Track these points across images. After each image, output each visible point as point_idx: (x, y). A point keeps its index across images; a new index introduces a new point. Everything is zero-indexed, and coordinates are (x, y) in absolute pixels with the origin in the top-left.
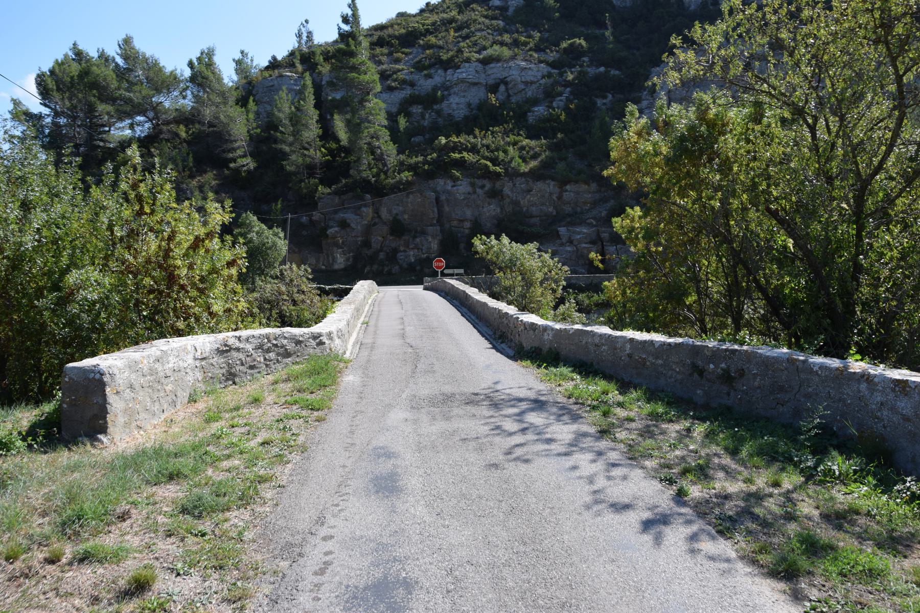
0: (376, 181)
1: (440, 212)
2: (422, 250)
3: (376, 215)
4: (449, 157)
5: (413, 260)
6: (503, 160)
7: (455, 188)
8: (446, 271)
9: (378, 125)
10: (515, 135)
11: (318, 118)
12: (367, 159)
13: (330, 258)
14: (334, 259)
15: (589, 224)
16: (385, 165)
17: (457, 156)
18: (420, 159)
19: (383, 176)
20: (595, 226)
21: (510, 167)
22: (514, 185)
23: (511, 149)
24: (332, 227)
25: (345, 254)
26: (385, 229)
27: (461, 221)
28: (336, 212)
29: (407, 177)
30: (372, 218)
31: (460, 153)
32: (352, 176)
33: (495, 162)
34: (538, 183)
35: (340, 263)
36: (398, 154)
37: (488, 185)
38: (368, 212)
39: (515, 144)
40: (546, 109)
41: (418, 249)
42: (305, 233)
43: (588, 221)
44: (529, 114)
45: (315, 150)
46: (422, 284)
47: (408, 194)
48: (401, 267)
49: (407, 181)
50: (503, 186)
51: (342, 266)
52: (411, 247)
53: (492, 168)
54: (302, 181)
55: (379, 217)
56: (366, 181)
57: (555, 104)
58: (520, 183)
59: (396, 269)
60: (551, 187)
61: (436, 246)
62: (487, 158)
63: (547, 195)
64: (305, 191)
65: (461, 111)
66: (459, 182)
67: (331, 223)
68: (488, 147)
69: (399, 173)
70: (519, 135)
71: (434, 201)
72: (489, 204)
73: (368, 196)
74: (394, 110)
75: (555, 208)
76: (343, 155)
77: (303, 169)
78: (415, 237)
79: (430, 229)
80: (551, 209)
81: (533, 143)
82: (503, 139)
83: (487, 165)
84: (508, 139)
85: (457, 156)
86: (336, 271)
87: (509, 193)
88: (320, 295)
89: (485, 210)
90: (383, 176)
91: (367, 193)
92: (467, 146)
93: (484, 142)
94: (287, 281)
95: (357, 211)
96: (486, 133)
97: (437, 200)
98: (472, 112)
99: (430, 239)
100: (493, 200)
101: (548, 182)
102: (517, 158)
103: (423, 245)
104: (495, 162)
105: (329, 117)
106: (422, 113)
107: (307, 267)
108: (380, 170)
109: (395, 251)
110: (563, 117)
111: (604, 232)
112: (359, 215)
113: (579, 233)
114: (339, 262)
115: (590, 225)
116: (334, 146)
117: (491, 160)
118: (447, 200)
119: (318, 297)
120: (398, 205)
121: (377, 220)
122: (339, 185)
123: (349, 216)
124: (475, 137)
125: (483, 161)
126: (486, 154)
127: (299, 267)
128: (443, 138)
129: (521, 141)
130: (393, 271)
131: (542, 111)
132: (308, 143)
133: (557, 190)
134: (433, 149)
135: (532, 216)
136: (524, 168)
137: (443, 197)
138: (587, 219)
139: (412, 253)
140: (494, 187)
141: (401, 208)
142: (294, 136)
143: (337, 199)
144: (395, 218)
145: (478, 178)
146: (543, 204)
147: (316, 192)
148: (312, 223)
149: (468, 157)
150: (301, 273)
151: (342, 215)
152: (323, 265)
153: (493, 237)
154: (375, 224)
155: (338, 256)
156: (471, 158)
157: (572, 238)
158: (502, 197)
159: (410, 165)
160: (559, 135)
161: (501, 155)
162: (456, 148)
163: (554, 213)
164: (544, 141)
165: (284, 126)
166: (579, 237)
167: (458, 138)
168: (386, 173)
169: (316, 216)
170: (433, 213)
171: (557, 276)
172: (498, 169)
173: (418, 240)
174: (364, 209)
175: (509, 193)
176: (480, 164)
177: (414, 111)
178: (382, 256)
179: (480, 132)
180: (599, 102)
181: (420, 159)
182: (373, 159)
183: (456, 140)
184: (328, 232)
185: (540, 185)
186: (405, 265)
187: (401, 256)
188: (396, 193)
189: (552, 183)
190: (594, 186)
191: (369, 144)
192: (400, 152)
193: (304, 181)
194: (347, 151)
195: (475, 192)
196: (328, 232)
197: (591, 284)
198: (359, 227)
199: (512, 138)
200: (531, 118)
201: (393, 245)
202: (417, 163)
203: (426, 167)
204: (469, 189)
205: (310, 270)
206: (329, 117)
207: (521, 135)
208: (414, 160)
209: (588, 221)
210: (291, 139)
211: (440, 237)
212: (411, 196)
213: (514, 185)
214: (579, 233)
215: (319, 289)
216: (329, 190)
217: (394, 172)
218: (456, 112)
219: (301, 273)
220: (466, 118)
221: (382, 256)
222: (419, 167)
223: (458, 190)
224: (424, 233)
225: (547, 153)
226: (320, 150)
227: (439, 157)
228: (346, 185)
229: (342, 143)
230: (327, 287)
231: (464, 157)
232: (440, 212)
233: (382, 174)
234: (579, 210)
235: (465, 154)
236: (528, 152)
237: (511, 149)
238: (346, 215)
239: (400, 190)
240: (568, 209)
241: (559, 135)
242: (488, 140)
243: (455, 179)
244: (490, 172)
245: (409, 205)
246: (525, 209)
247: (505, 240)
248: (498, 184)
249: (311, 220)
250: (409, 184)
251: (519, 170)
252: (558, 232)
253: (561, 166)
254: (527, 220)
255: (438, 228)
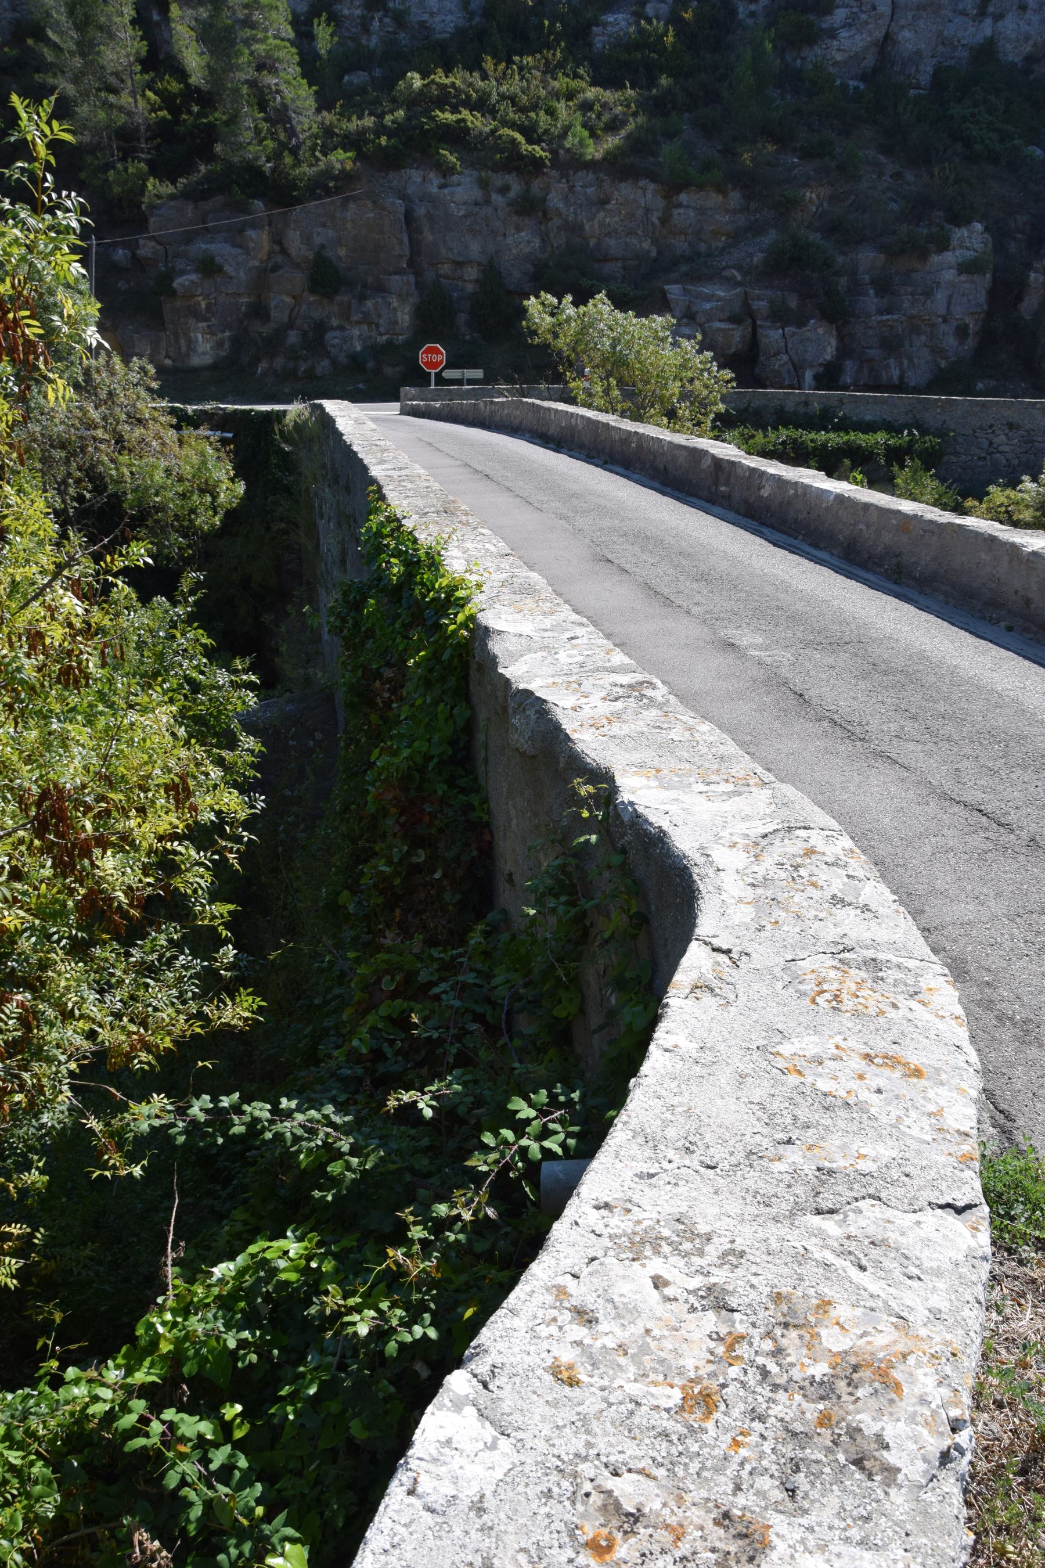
0: (274, 170)
1: (415, 245)
2: (377, 325)
3: (277, 248)
4: (432, 119)
5: (359, 348)
6: (546, 131)
7: (446, 191)
8: (448, 374)
9: (275, 37)
10: (568, 76)
11: (133, 13)
12: (250, 119)
13: (182, 342)
14: (191, 343)
15: (729, 279)
16: (292, 133)
17: (447, 117)
18: (369, 122)
19: (288, 160)
20: (739, 284)
21: (562, 147)
22: (571, 188)
23: (561, 106)
24: (183, 273)
25: (213, 334)
26: (298, 279)
27: (459, 264)
28: (189, 238)
29: (342, 162)
30: (270, 254)
31: (455, 110)
32: (219, 157)
33: (530, 133)
34: (623, 185)
35: (204, 353)
36: (318, 110)
37: (516, 187)
38: (260, 239)
39: (570, 96)
40: (632, 20)
41: (370, 324)
42: (122, 285)
43: (726, 273)
44: (595, 29)
45: (133, 94)
46: (394, 397)
47: (346, 200)
48: (334, 363)
49: (343, 171)
50: (547, 190)
51: (208, 360)
52: (355, 318)
53: (525, 148)
54: (108, 167)
55: (284, 251)
56: (253, 170)
57: (649, 10)
58: (584, 183)
59: (323, 366)
60: (649, 196)
61: (407, 318)
62: (513, 125)
63: (640, 213)
64: (117, 189)
65: (449, 17)
66: (455, 178)
67: (180, 264)
68: (513, 99)
69: (325, 155)
70: (576, 76)
71: (402, 218)
72: (519, 229)
73: (258, 204)
74: (303, 8)
75: (655, 242)
76: (196, 109)
77: (109, 138)
78: (362, 298)
79: (396, 282)
80: (646, 245)
81: (608, 95)
82: (545, 84)
83: (515, 140)
84: (556, 84)
85: (447, 117)
86: (195, 371)
87: (561, 205)
88: (178, 427)
89: (509, 240)
90: (288, 160)
91: (255, 196)
92: (468, 97)
93: (504, 88)
94: (103, 395)
95: (236, 236)
96: (507, 68)
97: (409, 217)
98: (471, 19)
99: (395, 304)
100: (527, 221)
101: (642, 183)
102: (579, 128)
103: (379, 316)
104: (530, 133)
105: (156, 17)
106: (363, 17)
107: (144, 362)
108: (283, 146)
109: (321, 328)
110: (670, 39)
111: (759, 299)
112: (240, 246)
113: (709, 298)
114: (201, 350)
115: (732, 283)
116: (175, 87)
117: (522, 130)
118: (430, 217)
119: (172, 432)
120: (324, 225)
121: (279, 259)
122: (194, 178)
123: (220, 249)
124: (485, 77)
125: (506, 131)
126: (511, 115)
127: (126, 361)
128: (417, 75)
129: (583, 91)
130: (319, 371)
131: (623, 24)
132: (116, 74)
133: (660, 203)
134: (394, 100)
135: (606, 259)
136: (594, 151)
137: (421, 211)
138: (725, 268)
139: (356, 332)
140: (528, 191)
141: (331, 233)
142: (83, 55)
143: (190, 209)
144: (319, 255)
145: (495, 170)
146: (631, 233)
147: (142, 194)
148: (138, 263)
149: (476, 122)
150: (134, 377)
151: (204, 246)
152: (168, 356)
153: (569, 298)
154: (275, 268)
155: (200, 336)
156: (478, 124)
157: (694, 309)
158: (545, 213)
159: (347, 136)
160: (664, 81)
161: (543, 119)
162: (446, 99)
163: (654, 254)
164: (630, 92)
165: (56, 26)
166: (708, 306)
167: (447, 77)
168: (294, 152)
169: (147, 248)
170: (399, 247)
171: (705, 392)
172: (538, 151)
173: (369, 304)
174: (251, 233)
175: (561, 205)
176: (500, 137)
177: (346, 12)
178: (293, 337)
179: (495, 65)
180: (741, 10)
181: (369, 122)
182: (265, 120)
183: (447, 81)
184: (175, 285)
185: (626, 190)
186: (342, 359)
187: (332, 338)
188: (320, 198)
189: (652, 186)
190: (735, 197)
191: (252, 84)
192: (324, 104)
193: (114, 168)
194: (206, 99)
195: (488, 201)
196: (175, 285)
197: (746, 409)
198: (242, 274)
199: (561, 83)
200: (600, 40)
201: (317, 315)
202: (363, 132)
203: (383, 141)
204: (477, 194)
205: (152, 370)
206: (156, 17)
207: (582, 78)
208: (354, 125)
209: (726, 273)
210: (78, 62)
211: (414, 299)
212: (352, 206)
213: (571, 188)
214: (709, 298)
215: (173, 411)
216: (170, 189)
217: (313, 149)
218: (437, 19)
219: (134, 377)
220: (460, 33)
221: (293, 337)
222: (366, 142)
223: (452, 194)
224: (381, 289)
225: (639, 120)
226: (144, 95)
227: (408, 118)
228: (208, 178)
229: (193, 80)
230: (190, 409)
231: (464, 120)
232: (415, 245)
233: (286, 153)
234: (703, 247)
235: (465, 114)
236: (599, 116)
237: (561, 106)
238: (212, 247)
239: (328, 192)
240: (680, 245)
241: (664, 81)
242: (513, 86)
243: (446, 171)
244: (520, 157)
245: (349, 225)
246: (592, 242)
247: (601, 306)
248: (537, 185)
249: (134, 256)
250: (346, 178)
251: (581, 155)
252: (664, 294)
253: (668, 150)
254: (596, 266)
255: (412, 278)
